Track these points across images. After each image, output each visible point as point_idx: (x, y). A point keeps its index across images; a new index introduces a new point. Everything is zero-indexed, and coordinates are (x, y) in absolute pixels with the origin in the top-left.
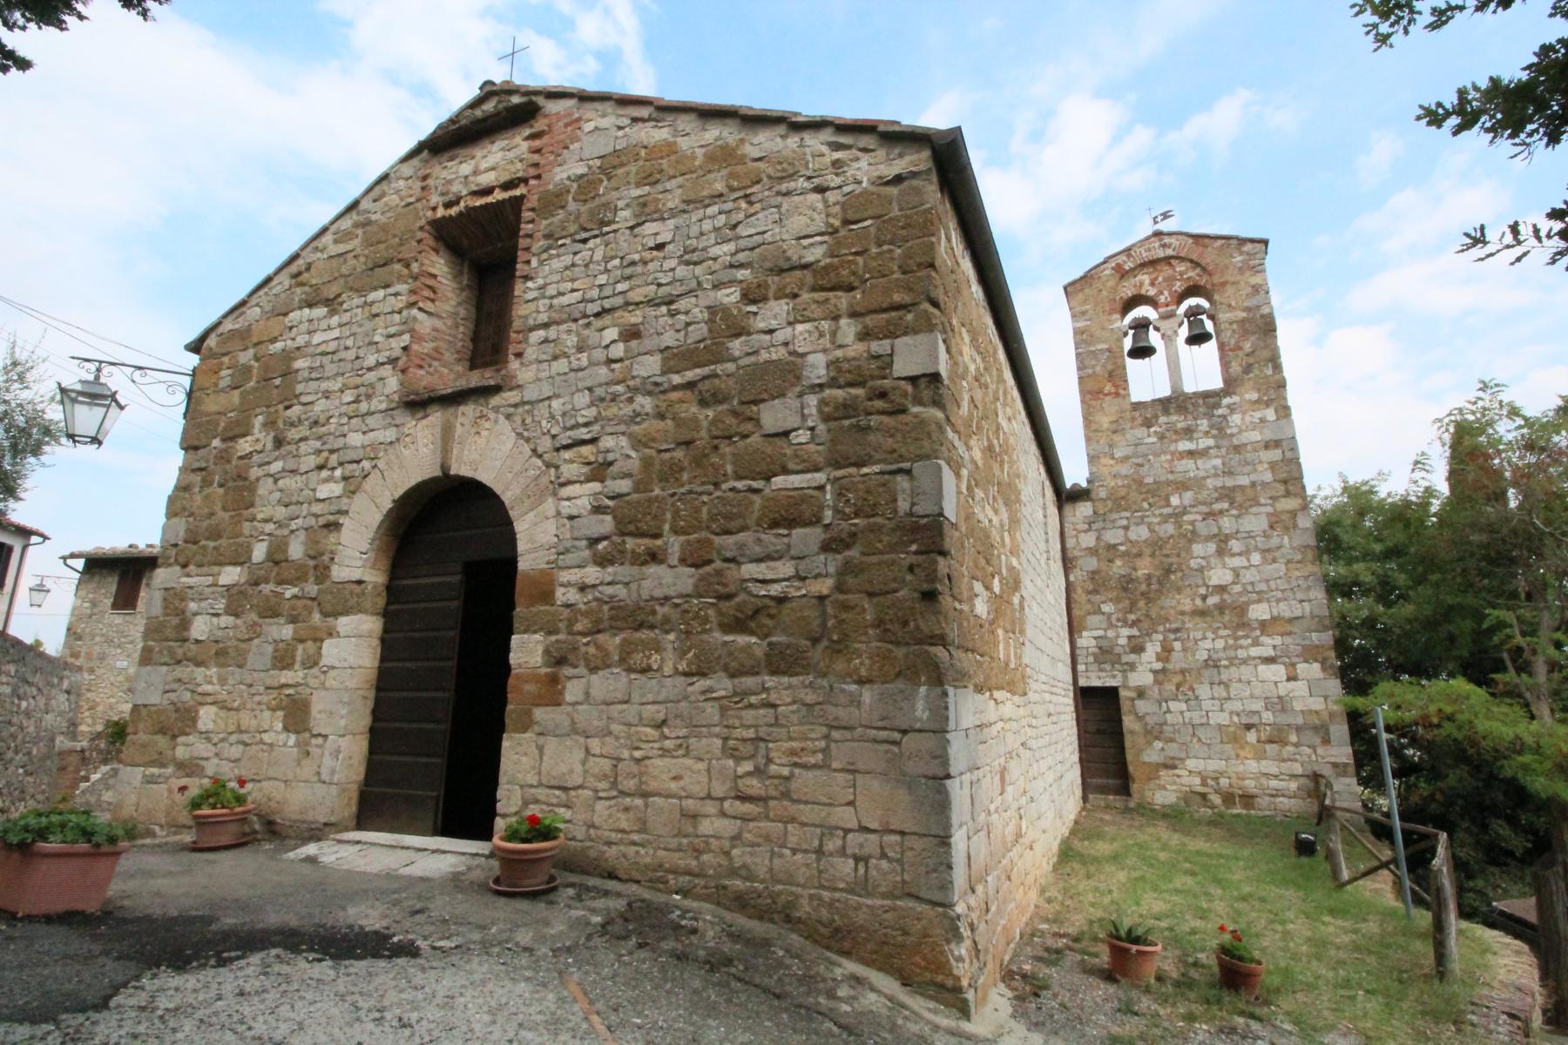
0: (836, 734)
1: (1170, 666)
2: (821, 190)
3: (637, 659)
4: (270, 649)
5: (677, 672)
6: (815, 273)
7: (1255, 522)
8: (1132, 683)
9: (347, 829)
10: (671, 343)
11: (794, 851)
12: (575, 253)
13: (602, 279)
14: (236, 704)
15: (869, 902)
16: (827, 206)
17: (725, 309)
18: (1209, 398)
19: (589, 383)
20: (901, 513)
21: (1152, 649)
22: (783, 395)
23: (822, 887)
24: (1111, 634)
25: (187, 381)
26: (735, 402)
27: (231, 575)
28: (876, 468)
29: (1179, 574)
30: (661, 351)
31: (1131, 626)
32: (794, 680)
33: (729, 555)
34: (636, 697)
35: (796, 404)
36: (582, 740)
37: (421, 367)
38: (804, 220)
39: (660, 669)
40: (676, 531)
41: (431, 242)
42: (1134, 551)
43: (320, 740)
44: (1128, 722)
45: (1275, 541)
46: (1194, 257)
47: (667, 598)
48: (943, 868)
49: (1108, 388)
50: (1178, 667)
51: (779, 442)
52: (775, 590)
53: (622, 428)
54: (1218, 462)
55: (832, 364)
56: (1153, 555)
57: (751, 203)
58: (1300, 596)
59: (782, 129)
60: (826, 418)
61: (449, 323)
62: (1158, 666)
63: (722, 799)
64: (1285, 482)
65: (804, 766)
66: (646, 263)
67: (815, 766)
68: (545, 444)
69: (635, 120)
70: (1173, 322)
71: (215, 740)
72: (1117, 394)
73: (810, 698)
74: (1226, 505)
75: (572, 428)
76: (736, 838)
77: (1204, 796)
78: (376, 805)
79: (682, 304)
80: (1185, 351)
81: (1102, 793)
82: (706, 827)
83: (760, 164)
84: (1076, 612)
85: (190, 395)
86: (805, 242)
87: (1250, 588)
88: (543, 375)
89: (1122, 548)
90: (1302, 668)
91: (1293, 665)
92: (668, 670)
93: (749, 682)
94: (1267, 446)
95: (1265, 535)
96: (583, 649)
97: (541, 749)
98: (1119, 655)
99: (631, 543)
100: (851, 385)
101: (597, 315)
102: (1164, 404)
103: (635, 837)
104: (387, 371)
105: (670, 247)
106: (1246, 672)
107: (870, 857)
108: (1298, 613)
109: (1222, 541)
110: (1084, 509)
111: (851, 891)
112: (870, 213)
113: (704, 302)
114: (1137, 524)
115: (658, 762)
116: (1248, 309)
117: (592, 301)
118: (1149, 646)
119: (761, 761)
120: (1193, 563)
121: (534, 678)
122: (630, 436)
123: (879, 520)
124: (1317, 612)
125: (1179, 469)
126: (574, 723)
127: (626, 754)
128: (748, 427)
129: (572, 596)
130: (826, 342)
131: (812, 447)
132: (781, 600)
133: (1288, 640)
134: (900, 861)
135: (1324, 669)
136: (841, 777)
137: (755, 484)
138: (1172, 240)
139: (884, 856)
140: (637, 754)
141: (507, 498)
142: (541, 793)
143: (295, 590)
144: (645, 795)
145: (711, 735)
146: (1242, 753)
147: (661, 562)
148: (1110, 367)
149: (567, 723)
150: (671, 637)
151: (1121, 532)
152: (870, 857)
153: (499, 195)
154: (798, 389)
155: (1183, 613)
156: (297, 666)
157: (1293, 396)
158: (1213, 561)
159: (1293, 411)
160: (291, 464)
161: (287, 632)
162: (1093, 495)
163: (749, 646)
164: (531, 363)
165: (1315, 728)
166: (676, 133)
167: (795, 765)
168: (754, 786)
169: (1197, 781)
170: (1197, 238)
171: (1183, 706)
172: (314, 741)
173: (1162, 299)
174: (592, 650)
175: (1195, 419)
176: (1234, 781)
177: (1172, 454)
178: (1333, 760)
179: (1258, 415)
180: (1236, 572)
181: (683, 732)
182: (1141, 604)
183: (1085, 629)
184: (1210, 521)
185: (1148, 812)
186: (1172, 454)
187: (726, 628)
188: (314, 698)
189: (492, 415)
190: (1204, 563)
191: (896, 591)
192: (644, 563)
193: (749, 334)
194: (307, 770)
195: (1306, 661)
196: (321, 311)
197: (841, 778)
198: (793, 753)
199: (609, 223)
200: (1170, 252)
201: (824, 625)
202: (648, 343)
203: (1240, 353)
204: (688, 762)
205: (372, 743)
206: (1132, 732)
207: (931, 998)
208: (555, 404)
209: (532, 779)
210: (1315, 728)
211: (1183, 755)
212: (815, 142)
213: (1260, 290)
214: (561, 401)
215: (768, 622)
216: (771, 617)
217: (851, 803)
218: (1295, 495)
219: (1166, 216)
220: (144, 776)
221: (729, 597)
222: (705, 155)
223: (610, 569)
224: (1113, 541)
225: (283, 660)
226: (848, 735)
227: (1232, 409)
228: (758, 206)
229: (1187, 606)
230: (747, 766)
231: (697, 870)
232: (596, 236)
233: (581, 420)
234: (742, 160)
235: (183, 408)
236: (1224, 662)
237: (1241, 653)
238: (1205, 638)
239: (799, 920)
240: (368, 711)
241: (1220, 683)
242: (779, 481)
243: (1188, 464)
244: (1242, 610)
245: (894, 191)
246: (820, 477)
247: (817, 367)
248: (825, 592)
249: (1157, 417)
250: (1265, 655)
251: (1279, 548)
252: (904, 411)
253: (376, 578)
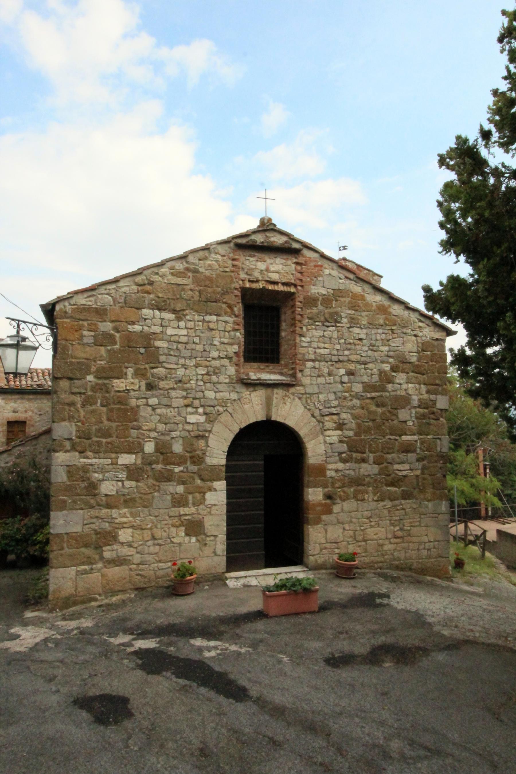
0: (422, 516)
2: (415, 336)
3: (360, 496)
4: (169, 498)
5: (373, 500)
6: (414, 366)
10: (366, 380)
12: (324, 331)
13: (338, 347)
14: (149, 526)
17: (385, 372)
19: (334, 390)
22: (404, 408)
26: (389, 407)
27: (126, 459)
30: (362, 383)
32: (410, 501)
33: (389, 461)
34: (360, 509)
35: (409, 412)
36: (341, 525)
40: (371, 452)
43: (212, 538)
47: (369, 475)
51: (404, 424)
52: (404, 473)
55: (419, 400)
57: (393, 333)
60: (417, 418)
63: (390, 539)
65: (414, 526)
66: (355, 345)
67: (417, 526)
68: (317, 413)
71: (136, 545)
75: (329, 408)
76: (395, 550)
78: (236, 559)
79: (370, 366)
82: (386, 548)
88: (314, 382)
92: (370, 500)
93: (397, 502)
96: (338, 493)
97: (326, 531)
99: (354, 455)
100: (424, 408)
103: (363, 554)
104: (226, 362)
105: (364, 341)
115: (369, 530)
117: (334, 355)
119: (401, 526)
121: (319, 504)
122: (352, 414)
126: (338, 520)
127: (358, 528)
128: (394, 417)
129: (333, 474)
130: (417, 392)
131: (413, 427)
132: (405, 476)
139: (434, 548)
140: (362, 528)
141: (302, 433)
142: (328, 545)
143: (181, 468)
144: (365, 541)
145: (386, 520)
147: (366, 462)
149: (336, 520)
150: (371, 488)
151: (204, 356)
153: (280, 288)
154: (409, 407)
156: (190, 505)
160: (165, 401)
161: (180, 489)
163: (396, 491)
164: (307, 376)
166: (364, 291)
167: (411, 526)
168: (400, 534)
172: (208, 539)
174: (342, 494)
181: (377, 520)
187: (388, 485)
188: (206, 519)
189: (292, 397)
192: (360, 463)
193: (393, 383)
194: (207, 551)
196: (168, 316)
197: (424, 528)
198: (411, 523)
199: (339, 322)
201: (418, 484)
202: (358, 379)
204: (379, 529)
208: (320, 396)
209: (323, 541)
214: (323, 395)
217: (426, 535)
220: (77, 571)
221: (390, 475)
222: (376, 306)
223: (347, 464)
225: (179, 502)
228: (395, 335)
230: (397, 528)
232: (333, 326)
233: (332, 405)
234: (390, 313)
242: (404, 437)
246: (416, 437)
247: (415, 400)
248: (418, 474)
252: (438, 419)
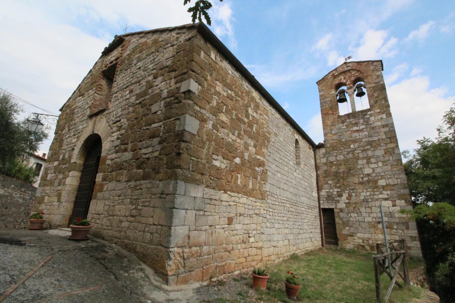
0: (153, 196)
1: (351, 201)
7: (380, 152)
8: (338, 207)
9: (64, 227)
11: (139, 231)
15: (152, 246)
16: (173, 50)
18: (364, 112)
20: (176, 131)
21: (345, 196)
23: (143, 242)
24: (331, 191)
25: (57, 118)
28: (173, 119)
29: (354, 171)
31: (338, 188)
37: (95, 108)
38: (168, 54)
39: (122, 181)
40: (131, 142)
41: (102, 77)
42: (339, 163)
44: (337, 220)
45: (387, 158)
46: (357, 69)
48: (168, 236)
49: (330, 112)
50: (354, 202)
53: (125, 117)
54: (366, 133)
55: (168, 92)
56: (345, 165)
58: (396, 177)
59: (167, 32)
61: (105, 97)
62: (347, 201)
63: (127, 216)
64: (390, 138)
69: (141, 37)
70: (352, 90)
72: (333, 114)
73: (149, 186)
74: (369, 147)
77: (363, 246)
80: (357, 99)
81: (329, 244)
83: (162, 42)
84: (320, 184)
85: (58, 121)
86: (167, 60)
87: (378, 175)
89: (335, 163)
90: (398, 202)
91: (395, 201)
93: (138, 182)
94: (383, 126)
95: (383, 156)
98: (334, 198)
101: (126, 88)
102: (348, 116)
103: (109, 228)
106: (378, 203)
107: (154, 233)
108: (396, 183)
109: (368, 159)
110: (323, 151)
111: (148, 243)
112: (182, 49)
113: (146, 81)
114: (340, 155)
116: (376, 83)
118: (344, 195)
120: (358, 167)
123: (171, 133)
124: (402, 182)
125: (353, 136)
132: (148, 159)
133: (393, 192)
134: (160, 234)
135: (406, 202)
136: (151, 209)
137: (148, 127)
138: (350, 64)
139: (157, 232)
146: (377, 232)
148: (331, 105)
150: (126, 171)
151: (335, 157)
152: (154, 233)
153: (114, 62)
155: (355, 183)
157: (392, 110)
158: (365, 166)
159: (392, 114)
162: (326, 146)
165: (403, 223)
167: (143, 206)
169: (361, 241)
170: (358, 63)
171: (356, 215)
173: (348, 83)
175: (359, 120)
176: (374, 241)
177: (351, 131)
178: (410, 235)
179: (380, 117)
180: (373, 169)
182: (341, 181)
183: (323, 189)
184: (364, 152)
185: (343, 251)
186: (351, 131)
190: (362, 166)
191: (171, 153)
192: (124, 152)
195: (399, 199)
196: (81, 97)
200: (349, 68)
203: (373, 97)
205: (74, 205)
206: (339, 224)
207: (160, 277)
210: (403, 223)
211: (356, 232)
212: (174, 34)
213: (380, 77)
215: (145, 165)
216: (146, 164)
217: (152, 217)
218: (394, 142)
219: (349, 58)
224: (332, 160)
226: (155, 196)
227: (371, 115)
229: (356, 180)
231: (119, 237)
235: (56, 124)
236: (370, 200)
237: (376, 197)
238: (363, 192)
239: (137, 252)
240: (74, 197)
241: (368, 208)
242: (153, 126)
243: (356, 134)
244: (376, 182)
245: (188, 42)
247: (165, 94)
248: (157, 155)
249: (346, 120)
250: (384, 197)
251: (388, 160)
252: (181, 102)
253: (80, 162)
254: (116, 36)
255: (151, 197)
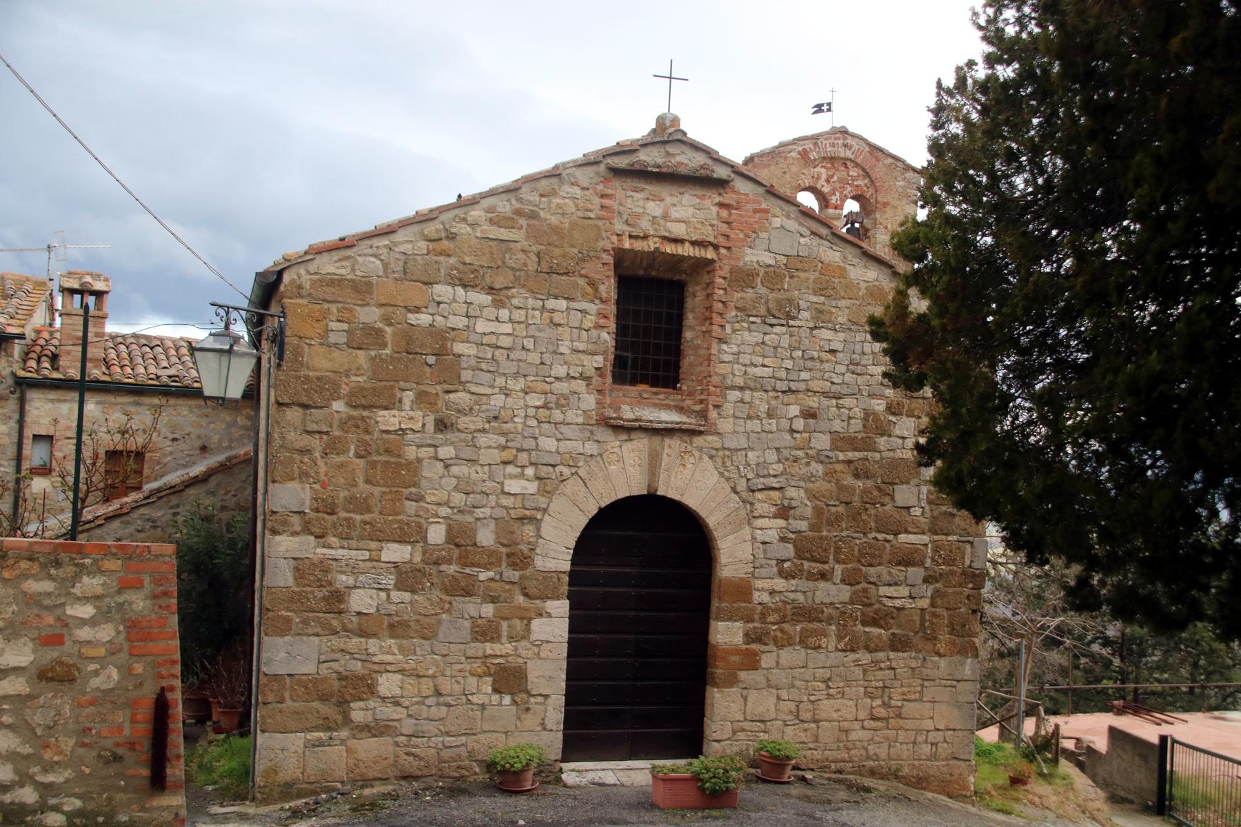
0: (926, 683)
167: (904, 700)
200: (849, 154)
242: (903, 537)
254: (676, 120)
255: (922, 685)
